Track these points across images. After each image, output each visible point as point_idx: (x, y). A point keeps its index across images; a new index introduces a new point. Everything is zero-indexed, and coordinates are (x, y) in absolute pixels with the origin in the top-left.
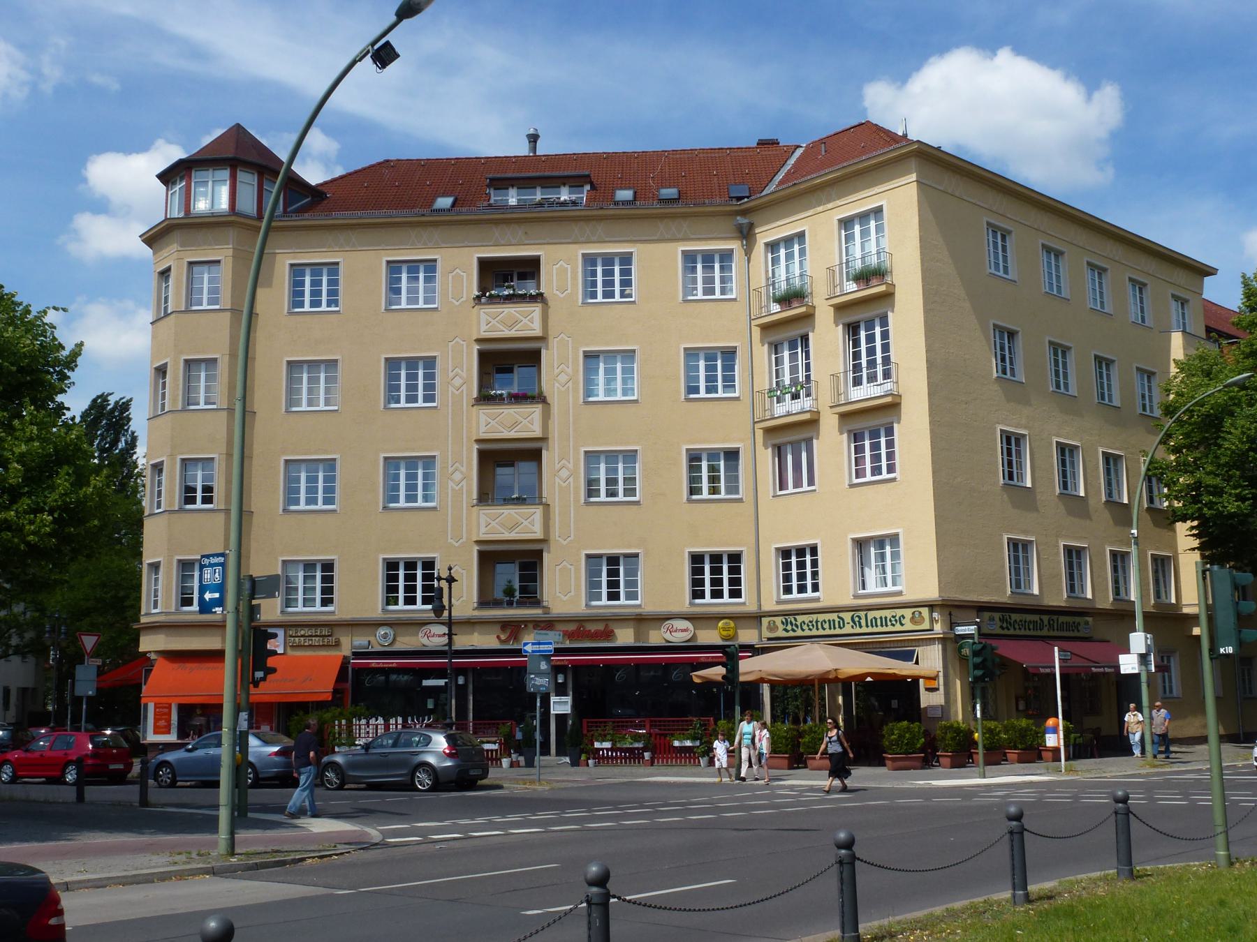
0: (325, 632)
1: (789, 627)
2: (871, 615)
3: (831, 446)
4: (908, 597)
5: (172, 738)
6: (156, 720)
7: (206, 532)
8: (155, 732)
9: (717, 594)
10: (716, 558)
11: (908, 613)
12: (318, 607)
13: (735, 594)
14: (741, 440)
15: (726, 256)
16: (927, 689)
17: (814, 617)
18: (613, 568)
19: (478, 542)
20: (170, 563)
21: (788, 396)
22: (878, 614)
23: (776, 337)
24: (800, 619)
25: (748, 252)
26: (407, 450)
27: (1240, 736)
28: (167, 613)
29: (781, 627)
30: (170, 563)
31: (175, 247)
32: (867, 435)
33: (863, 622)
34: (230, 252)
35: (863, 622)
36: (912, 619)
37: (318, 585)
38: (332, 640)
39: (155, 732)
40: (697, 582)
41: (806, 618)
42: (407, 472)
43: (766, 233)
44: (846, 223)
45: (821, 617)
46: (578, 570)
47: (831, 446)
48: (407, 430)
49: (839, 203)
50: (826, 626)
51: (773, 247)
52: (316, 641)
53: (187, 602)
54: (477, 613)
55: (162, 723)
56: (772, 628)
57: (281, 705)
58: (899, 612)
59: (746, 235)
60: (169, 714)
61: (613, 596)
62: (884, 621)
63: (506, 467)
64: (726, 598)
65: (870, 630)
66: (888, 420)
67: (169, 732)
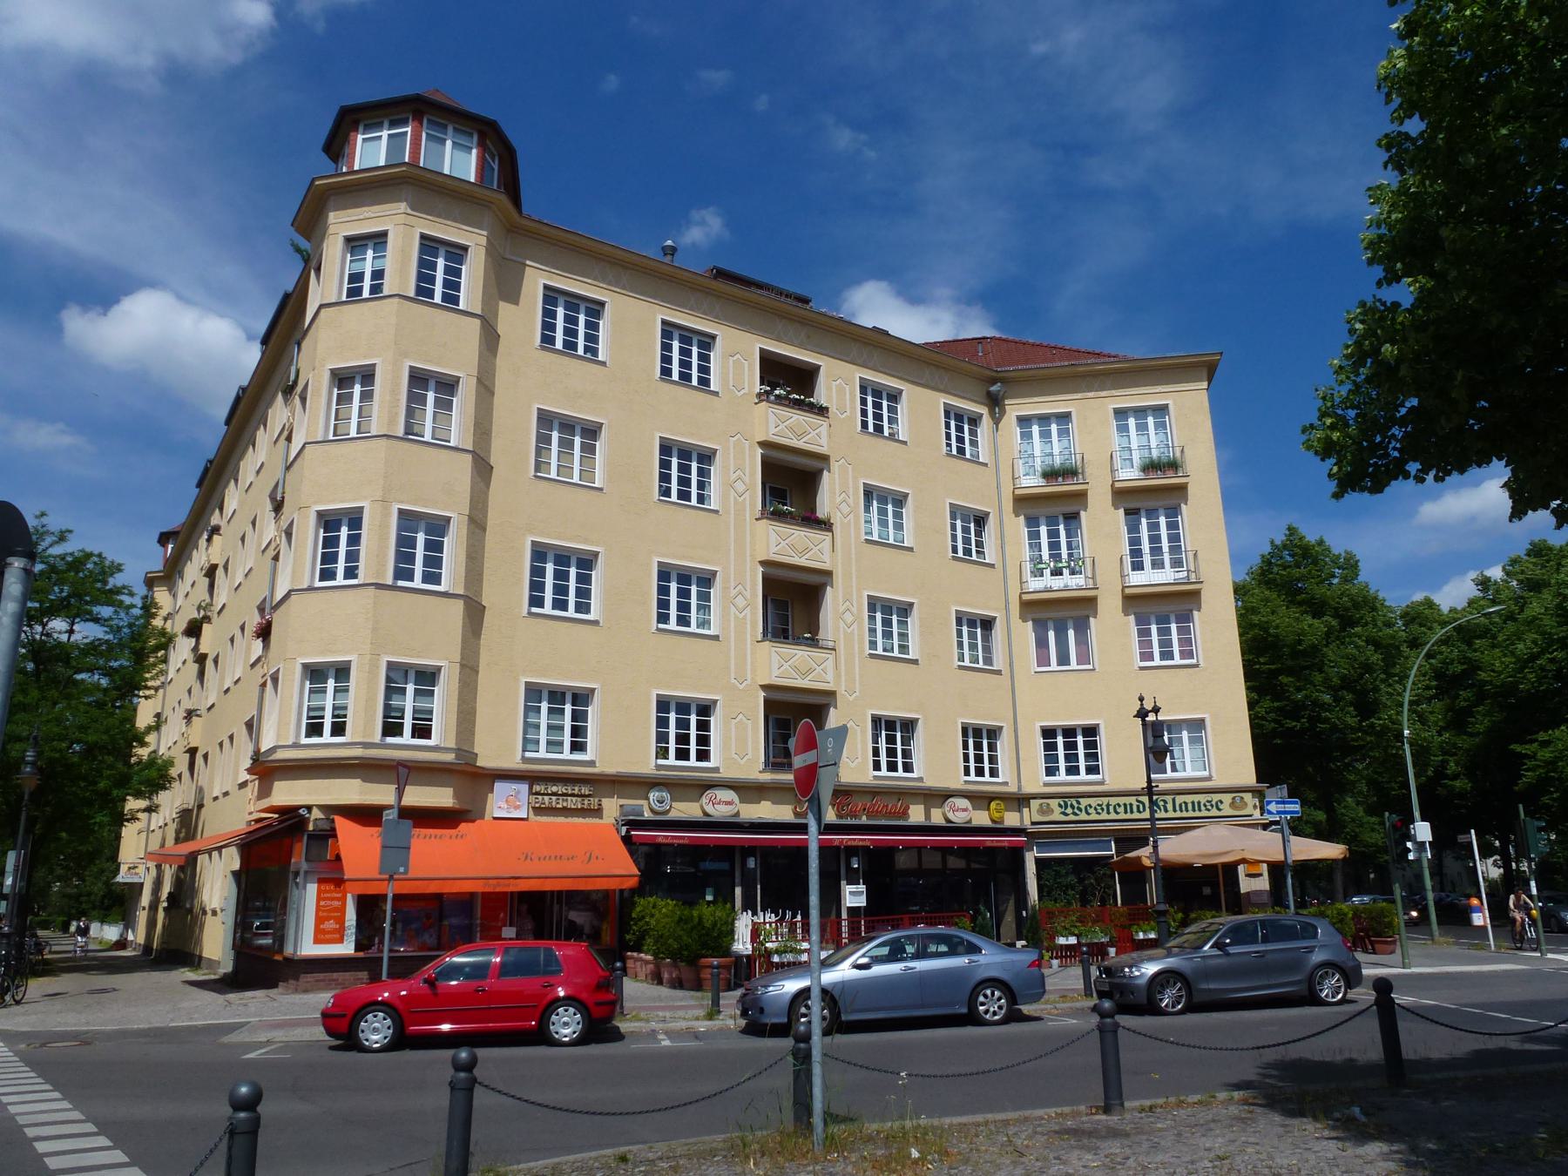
0: (585, 790)
1: (1069, 810)
2: (1180, 799)
3: (1112, 629)
4: (1218, 782)
5: (347, 948)
6: (319, 920)
7: (348, 625)
8: (317, 941)
9: (683, 754)
10: (1069, 732)
11: (1227, 798)
12: (567, 754)
13: (703, 755)
14: (997, 610)
15: (974, 421)
16: (1248, 875)
17: (1105, 800)
18: (894, 731)
19: (764, 687)
20: (374, 666)
21: (1047, 572)
22: (1189, 798)
23: (1033, 512)
24: (1084, 802)
25: (997, 421)
26: (684, 558)
27: (1558, 931)
28: (366, 745)
29: (1058, 810)
30: (374, 666)
31: (403, 206)
32: (1173, 618)
33: (1170, 807)
34: (484, 241)
35: (1170, 807)
36: (1233, 805)
37: (568, 722)
38: (594, 802)
39: (317, 941)
40: (1051, 758)
41: (1093, 802)
42: (682, 587)
43: (1016, 408)
44: (1121, 414)
45: (1114, 801)
46: (864, 732)
47: (1112, 629)
48: (681, 537)
49: (1114, 392)
50: (1121, 810)
51: (1024, 421)
52: (571, 803)
53: (315, 729)
54: (768, 777)
55: (330, 925)
56: (1045, 810)
57: (524, 897)
58: (1216, 797)
59: (995, 403)
60: (343, 910)
61: (683, 754)
62: (1197, 806)
63: (792, 603)
64: (1083, 776)
65: (1178, 814)
66: (1188, 607)
67: (341, 941)
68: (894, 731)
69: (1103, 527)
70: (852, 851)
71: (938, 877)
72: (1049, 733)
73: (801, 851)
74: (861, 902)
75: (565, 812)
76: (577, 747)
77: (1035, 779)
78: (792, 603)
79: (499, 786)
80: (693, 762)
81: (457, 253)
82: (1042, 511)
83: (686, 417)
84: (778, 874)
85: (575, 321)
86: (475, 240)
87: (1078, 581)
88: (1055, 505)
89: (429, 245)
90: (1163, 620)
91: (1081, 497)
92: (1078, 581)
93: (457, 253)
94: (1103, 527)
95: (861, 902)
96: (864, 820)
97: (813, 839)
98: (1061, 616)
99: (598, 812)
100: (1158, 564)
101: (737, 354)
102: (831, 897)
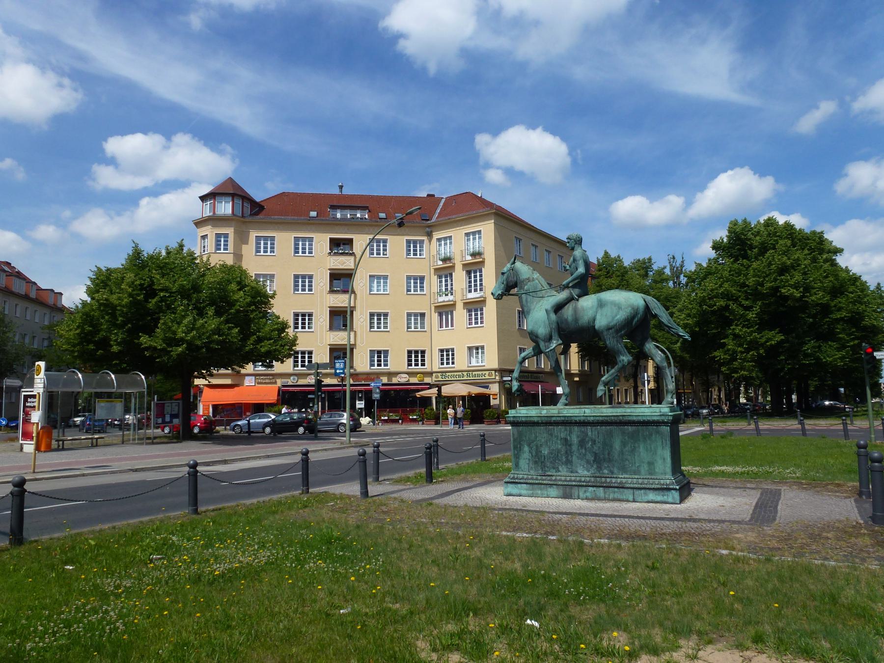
3: (460, 314)
11: (487, 373)
15: (422, 242)
25: (430, 241)
43: (437, 235)
44: (467, 235)
47: (460, 314)
51: (439, 240)
52: (267, 381)
59: (430, 235)
62: (478, 375)
68: (447, 354)
69: (460, 277)
70: (360, 391)
71: (400, 401)
72: (442, 351)
73: (345, 391)
74: (363, 406)
75: (265, 383)
76: (423, 365)
77: (436, 366)
78: (340, 318)
79: (247, 378)
80: (420, 366)
81: (226, 236)
82: (443, 273)
83: (303, 266)
84: (335, 400)
85: (267, 244)
86: (230, 231)
87: (450, 297)
88: (445, 272)
89: (218, 236)
90: (476, 310)
91: (453, 267)
92: (450, 297)
93: (226, 236)
94: (460, 277)
95: (363, 406)
96: (363, 382)
97: (348, 388)
98: (445, 311)
99: (275, 383)
100: (476, 290)
101: (321, 240)
102: (353, 406)
